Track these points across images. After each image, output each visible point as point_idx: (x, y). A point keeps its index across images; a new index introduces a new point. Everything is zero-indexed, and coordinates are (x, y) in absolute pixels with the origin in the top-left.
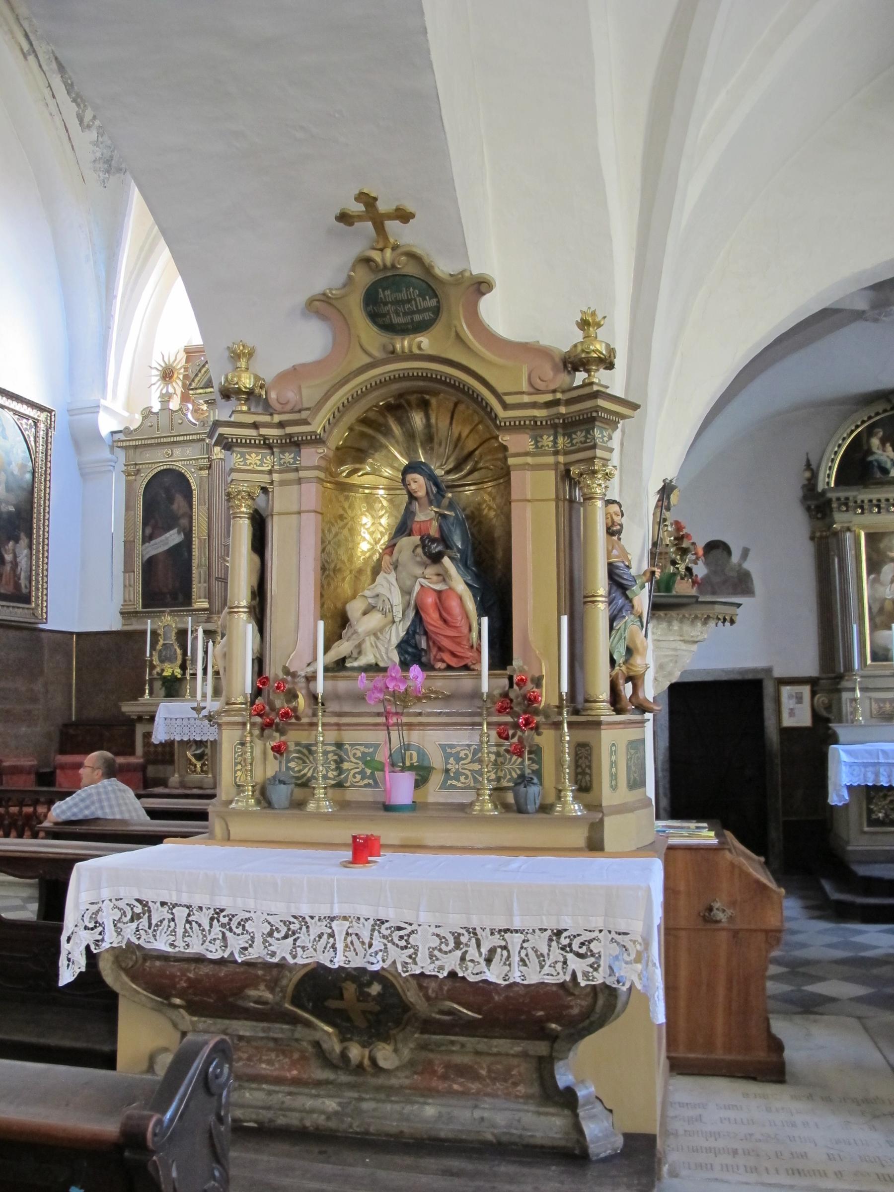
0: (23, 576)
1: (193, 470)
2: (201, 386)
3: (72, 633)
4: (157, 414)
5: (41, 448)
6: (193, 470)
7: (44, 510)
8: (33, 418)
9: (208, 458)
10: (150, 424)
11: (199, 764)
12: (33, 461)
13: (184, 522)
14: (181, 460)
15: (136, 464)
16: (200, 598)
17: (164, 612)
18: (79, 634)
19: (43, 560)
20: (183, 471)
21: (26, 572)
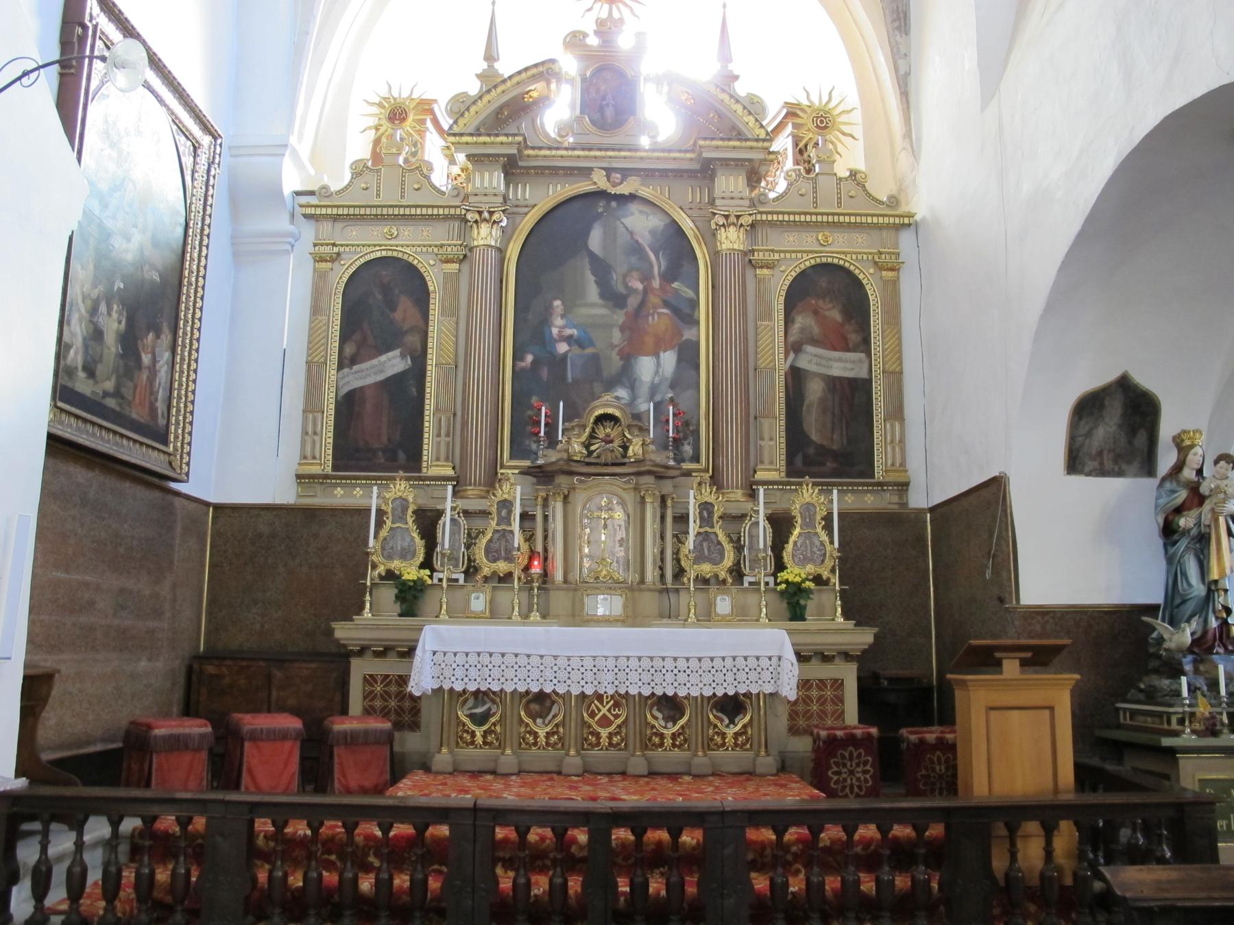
3: (207, 504)
6: (432, 262)
10: (363, 185)
11: (479, 732)
12: (188, 210)
13: (413, 340)
15: (334, 245)
16: (438, 459)
17: (394, 479)
18: (218, 508)
19: (188, 375)
20: (415, 262)
21: (164, 389)
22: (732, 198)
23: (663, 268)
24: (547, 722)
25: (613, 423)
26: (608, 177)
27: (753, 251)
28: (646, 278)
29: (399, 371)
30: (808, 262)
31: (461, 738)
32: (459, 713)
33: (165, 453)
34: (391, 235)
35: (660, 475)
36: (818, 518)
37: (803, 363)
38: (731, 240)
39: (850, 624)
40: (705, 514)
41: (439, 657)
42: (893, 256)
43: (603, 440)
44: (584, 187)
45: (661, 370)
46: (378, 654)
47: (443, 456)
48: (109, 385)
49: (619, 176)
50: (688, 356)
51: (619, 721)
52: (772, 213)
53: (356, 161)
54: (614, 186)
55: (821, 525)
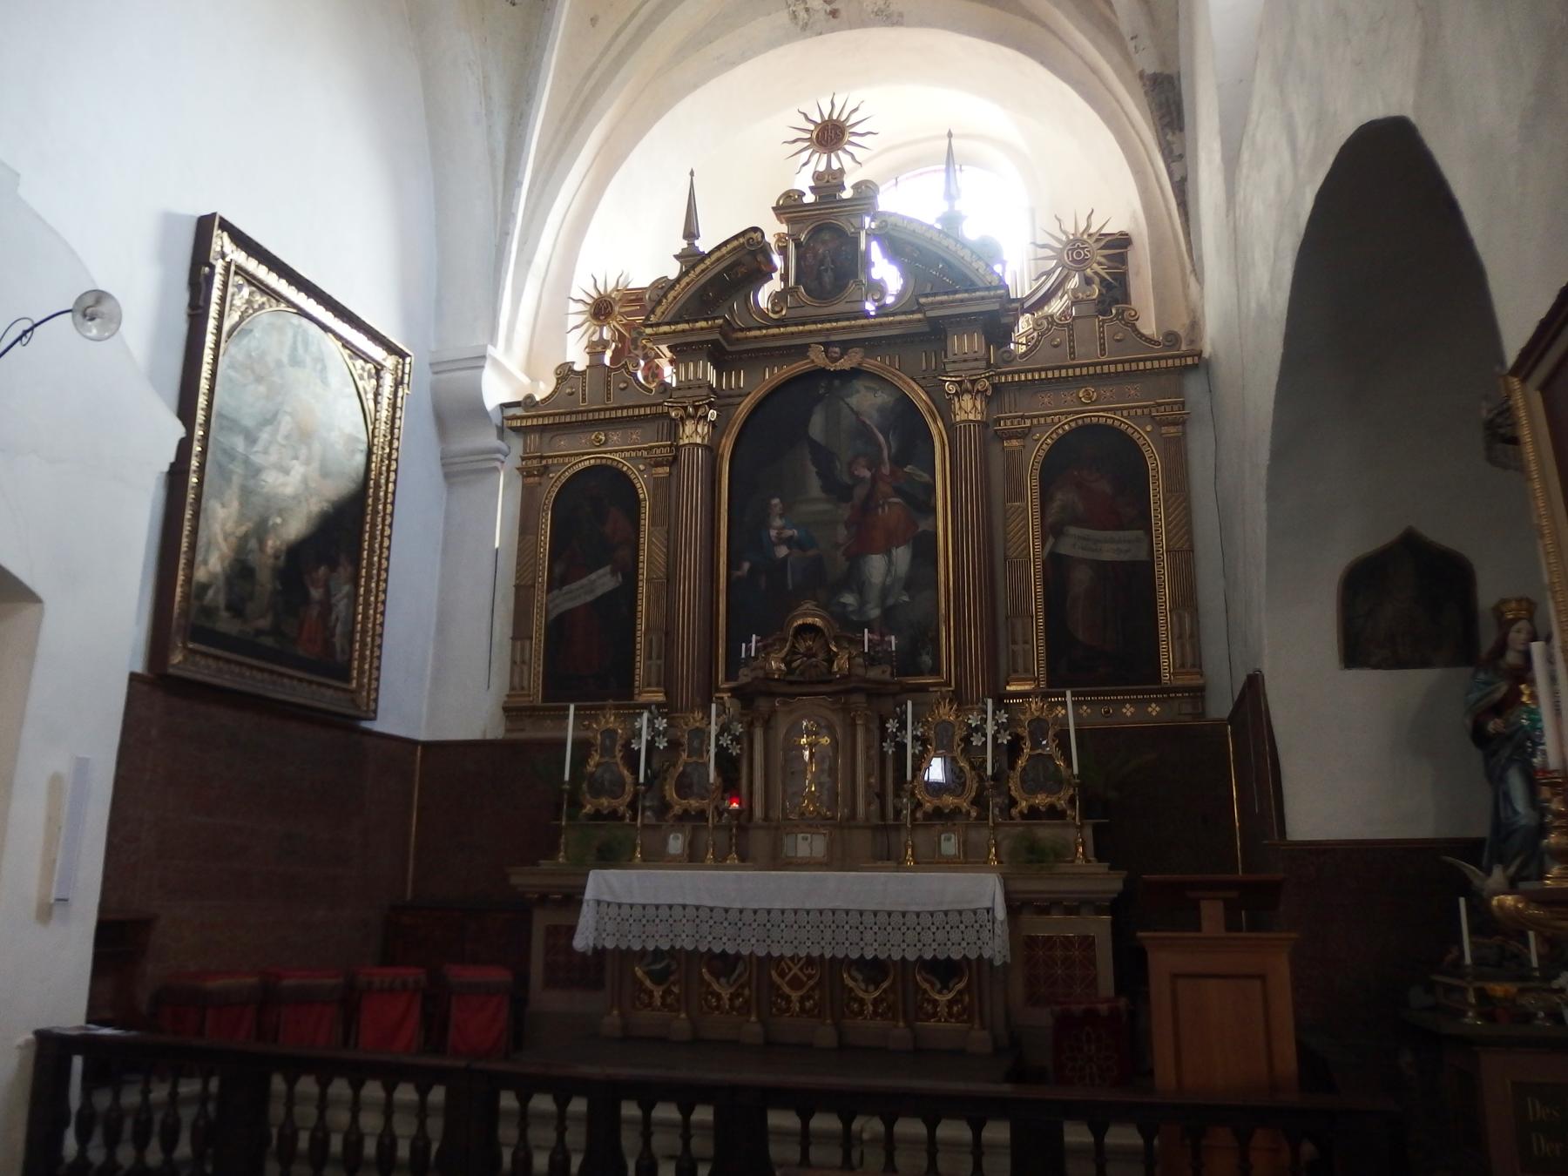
0: (339, 629)
1: (642, 467)
2: (666, 320)
3: (415, 743)
4: (583, 373)
5: (384, 414)
6: (642, 467)
7: (384, 520)
8: (374, 360)
9: (671, 446)
10: (568, 390)
11: (658, 993)
14: (622, 451)
15: (542, 458)
16: (649, 685)
17: (602, 708)
20: (625, 469)
22: (965, 361)
23: (893, 450)
24: (731, 982)
25: (813, 635)
26: (826, 352)
27: (998, 421)
28: (875, 464)
29: (610, 589)
30: (1066, 425)
31: (706, 1000)
32: (918, 978)
33: (345, 690)
34: (599, 442)
35: (875, 692)
36: (957, 738)
37: (1065, 549)
38: (968, 409)
39: (1103, 867)
40: (608, 742)
41: (604, 908)
42: (1167, 407)
43: (805, 655)
44: (800, 366)
45: (893, 569)
46: (1070, 911)
47: (654, 680)
48: (265, 623)
49: (837, 350)
50: (925, 549)
51: (811, 983)
52: (1019, 372)
53: (561, 365)
54: (832, 363)
55: (960, 748)
